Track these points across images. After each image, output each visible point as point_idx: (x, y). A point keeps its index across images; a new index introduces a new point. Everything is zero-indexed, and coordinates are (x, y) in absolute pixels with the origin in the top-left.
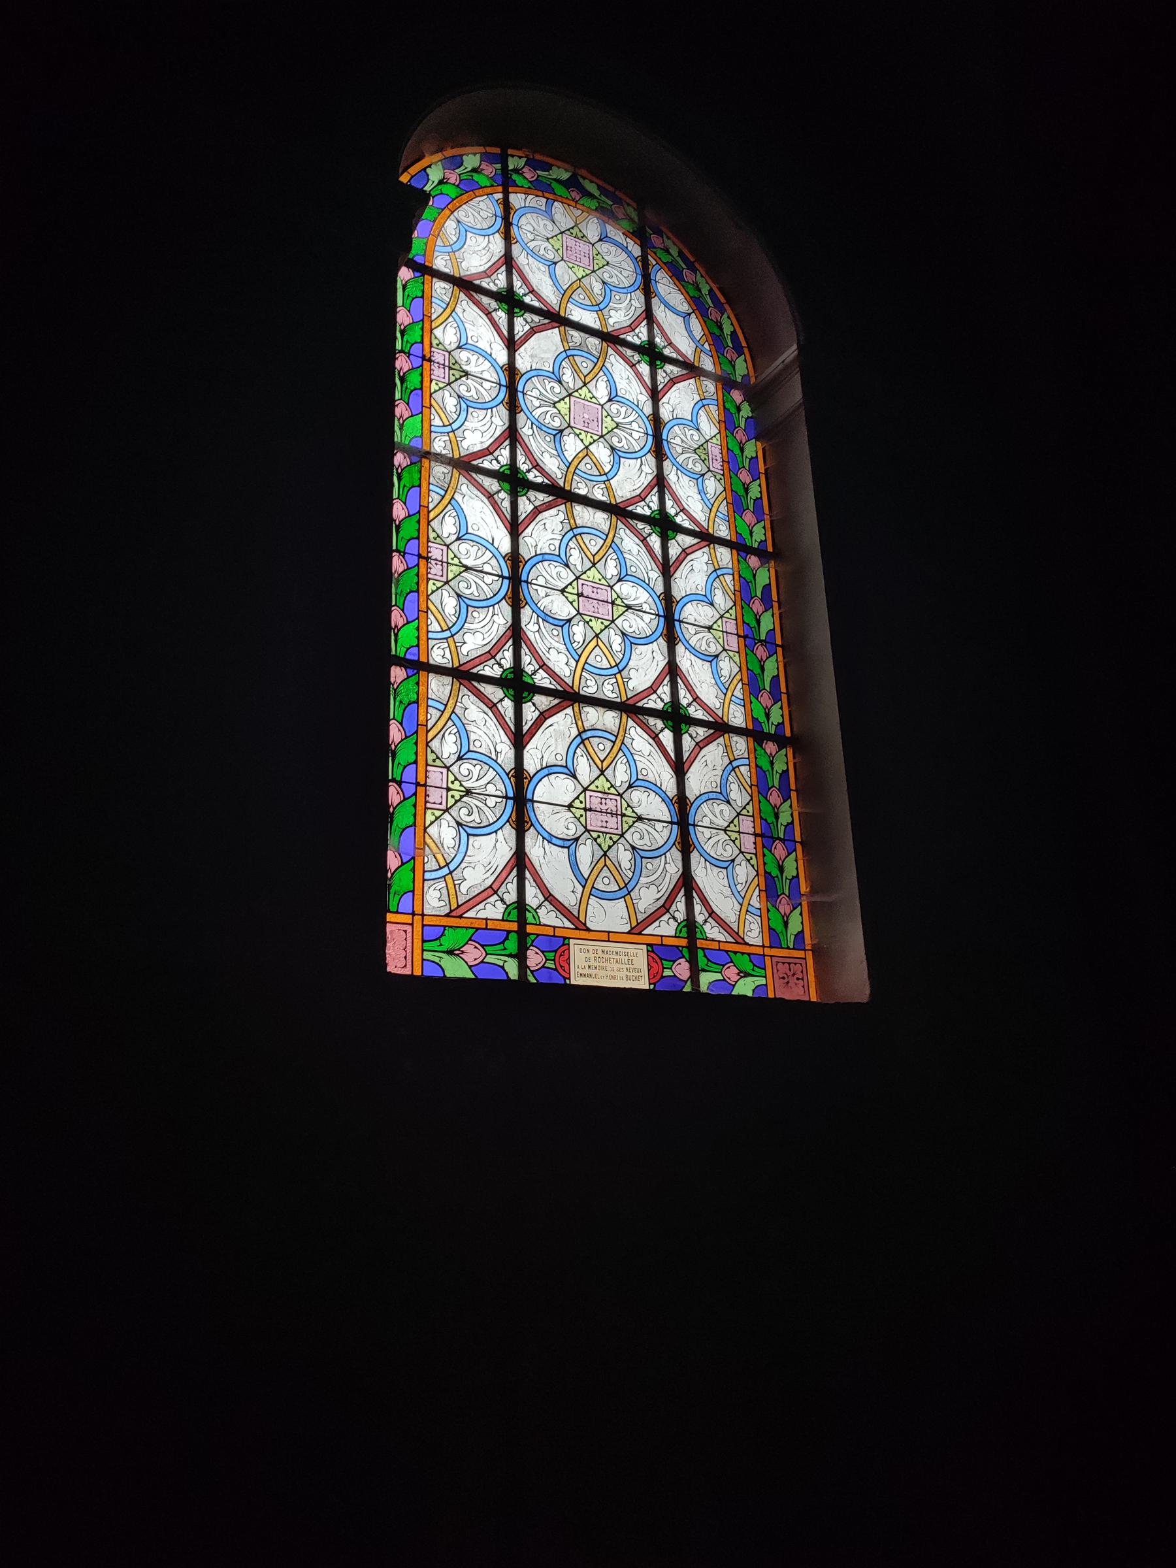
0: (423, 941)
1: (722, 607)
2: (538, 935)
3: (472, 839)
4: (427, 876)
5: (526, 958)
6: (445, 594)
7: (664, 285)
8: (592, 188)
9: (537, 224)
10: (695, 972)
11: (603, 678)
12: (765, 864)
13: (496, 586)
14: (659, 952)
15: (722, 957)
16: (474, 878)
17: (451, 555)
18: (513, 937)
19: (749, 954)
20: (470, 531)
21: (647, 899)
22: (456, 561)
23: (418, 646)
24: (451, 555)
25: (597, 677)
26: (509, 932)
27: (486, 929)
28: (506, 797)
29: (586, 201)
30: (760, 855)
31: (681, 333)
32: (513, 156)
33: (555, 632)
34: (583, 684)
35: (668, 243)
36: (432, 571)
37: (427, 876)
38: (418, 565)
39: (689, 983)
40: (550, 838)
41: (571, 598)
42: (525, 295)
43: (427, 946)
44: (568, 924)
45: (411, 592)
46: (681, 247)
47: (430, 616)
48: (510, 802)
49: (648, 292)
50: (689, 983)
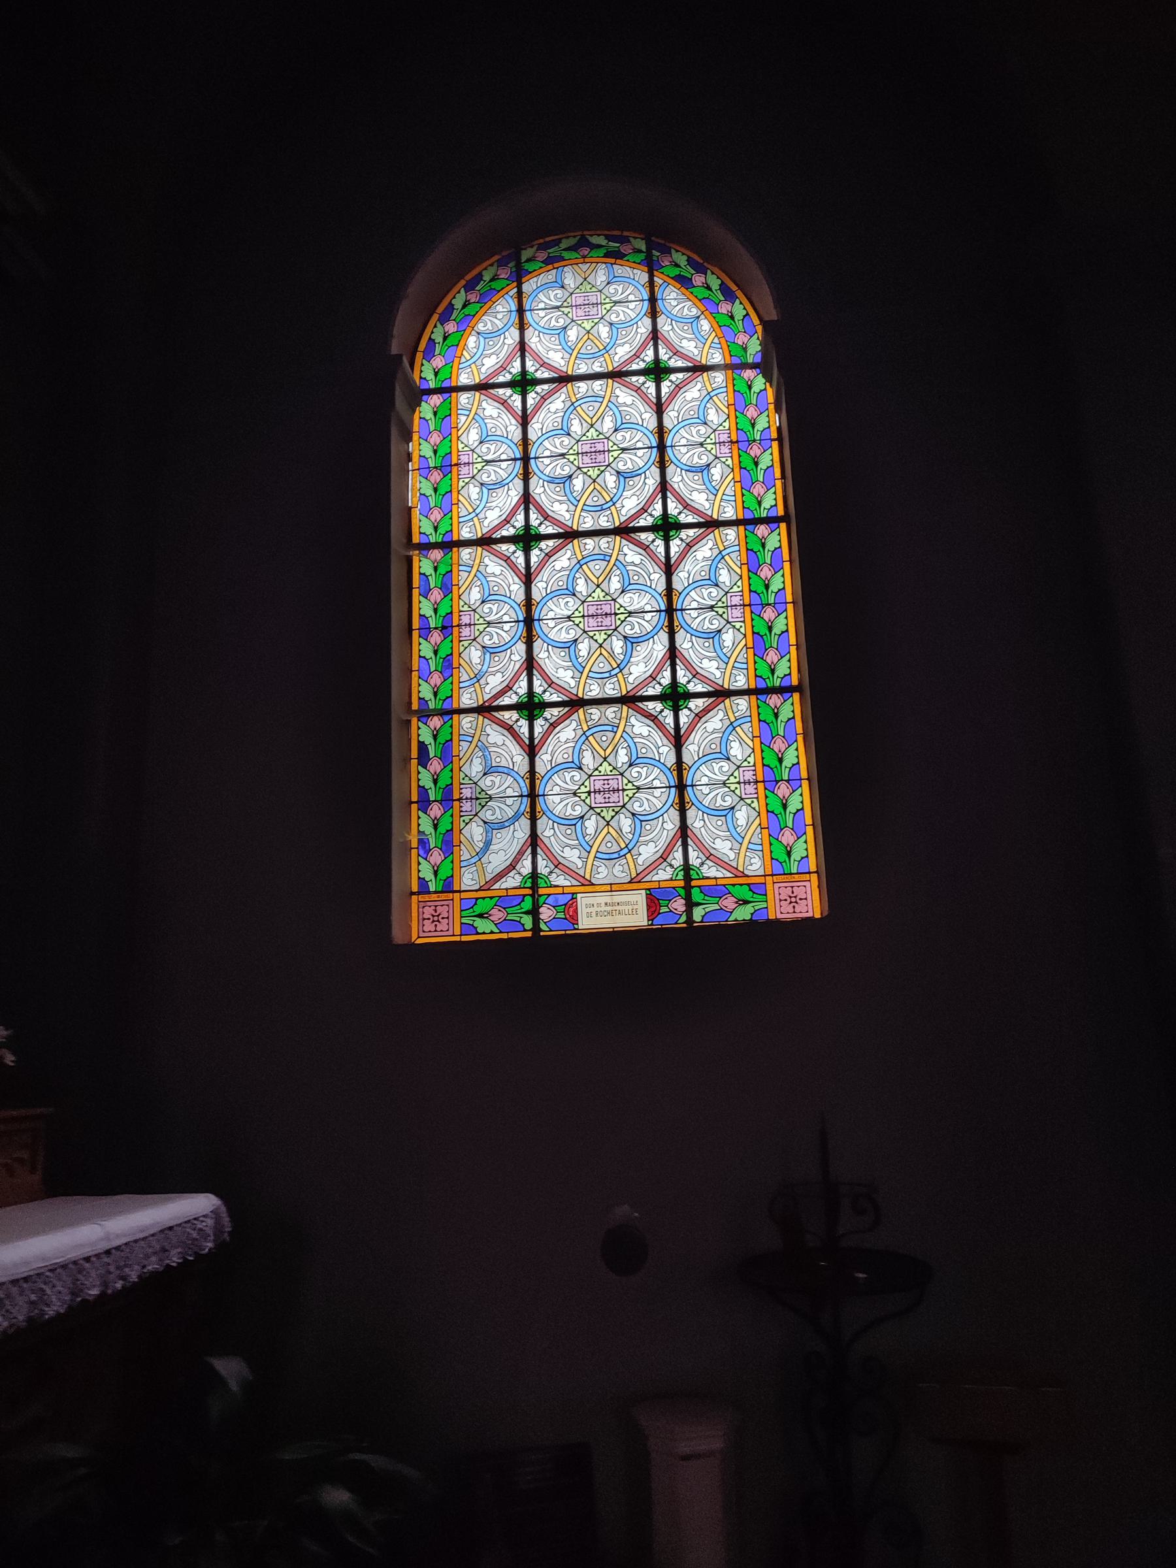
4: (737, 548)
6: (740, 757)
7: (672, 298)
8: (601, 241)
10: (690, 905)
11: (600, 722)
13: (697, 776)
14: (654, 902)
15: (716, 890)
16: (496, 861)
18: (529, 900)
19: (748, 885)
21: (647, 853)
25: (607, 722)
26: (524, 896)
28: (522, 796)
29: (594, 253)
33: (563, 654)
34: (747, 863)
37: (737, 548)
42: (536, 371)
44: (575, 883)
46: (689, 253)
47: (750, 735)
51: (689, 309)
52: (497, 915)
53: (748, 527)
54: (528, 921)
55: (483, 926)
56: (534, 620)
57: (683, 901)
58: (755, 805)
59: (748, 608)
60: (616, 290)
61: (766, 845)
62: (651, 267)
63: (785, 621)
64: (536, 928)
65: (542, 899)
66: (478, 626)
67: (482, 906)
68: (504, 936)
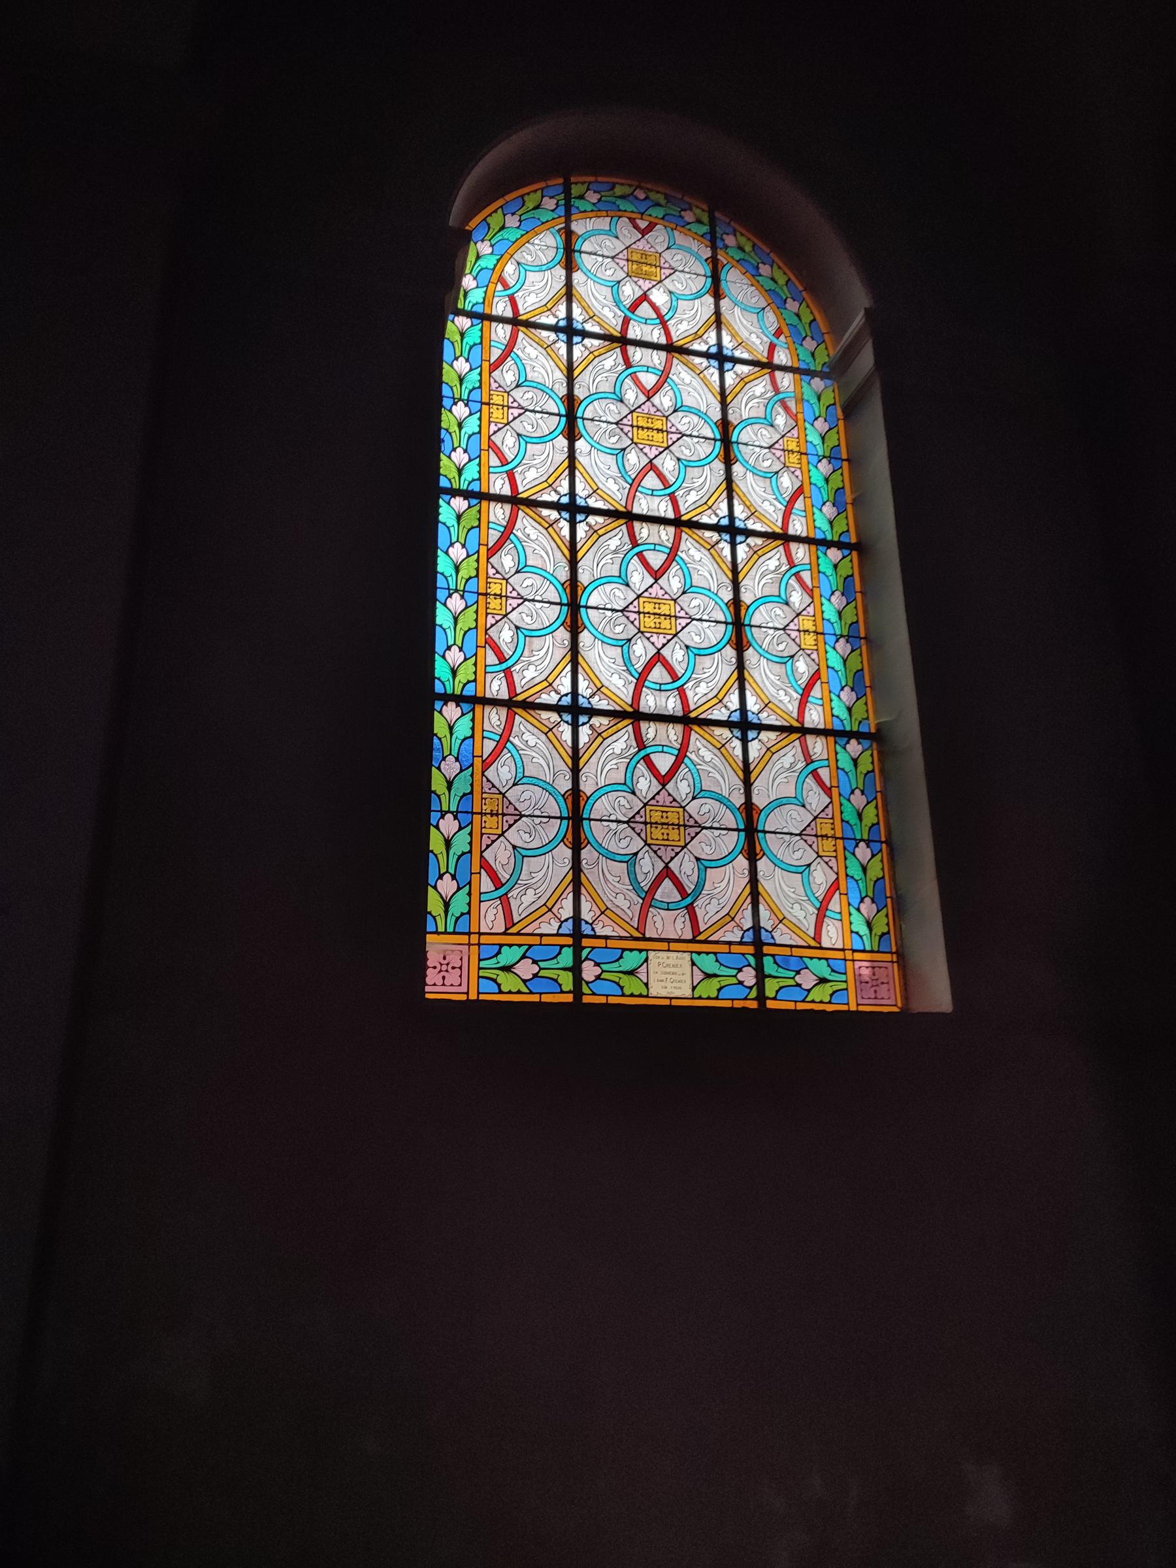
0: (480, 960)
1: (797, 605)
2: (593, 948)
3: (529, 446)
5: (580, 971)
7: (734, 281)
9: (603, 243)
12: (842, 813)
17: (511, 400)
20: (529, 378)
22: (515, 405)
23: (480, 479)
24: (510, 589)
27: (541, 994)
30: (822, 651)
31: (750, 327)
32: (576, 183)
35: (742, 240)
36: (491, 606)
38: (480, 411)
39: (755, 989)
40: (611, 856)
41: (626, 429)
43: (483, 964)
45: (469, 682)
48: (565, 609)
49: (717, 293)
50: (755, 989)
51: (756, 299)
52: (526, 969)
53: (820, 548)
54: (567, 981)
55: (508, 982)
56: (566, 416)
57: (753, 973)
58: (814, 656)
59: (840, 842)
60: (675, 258)
61: (826, 699)
62: (713, 241)
63: (885, 921)
64: (577, 991)
65: (585, 953)
66: (503, 610)
67: (508, 956)
68: (536, 998)
